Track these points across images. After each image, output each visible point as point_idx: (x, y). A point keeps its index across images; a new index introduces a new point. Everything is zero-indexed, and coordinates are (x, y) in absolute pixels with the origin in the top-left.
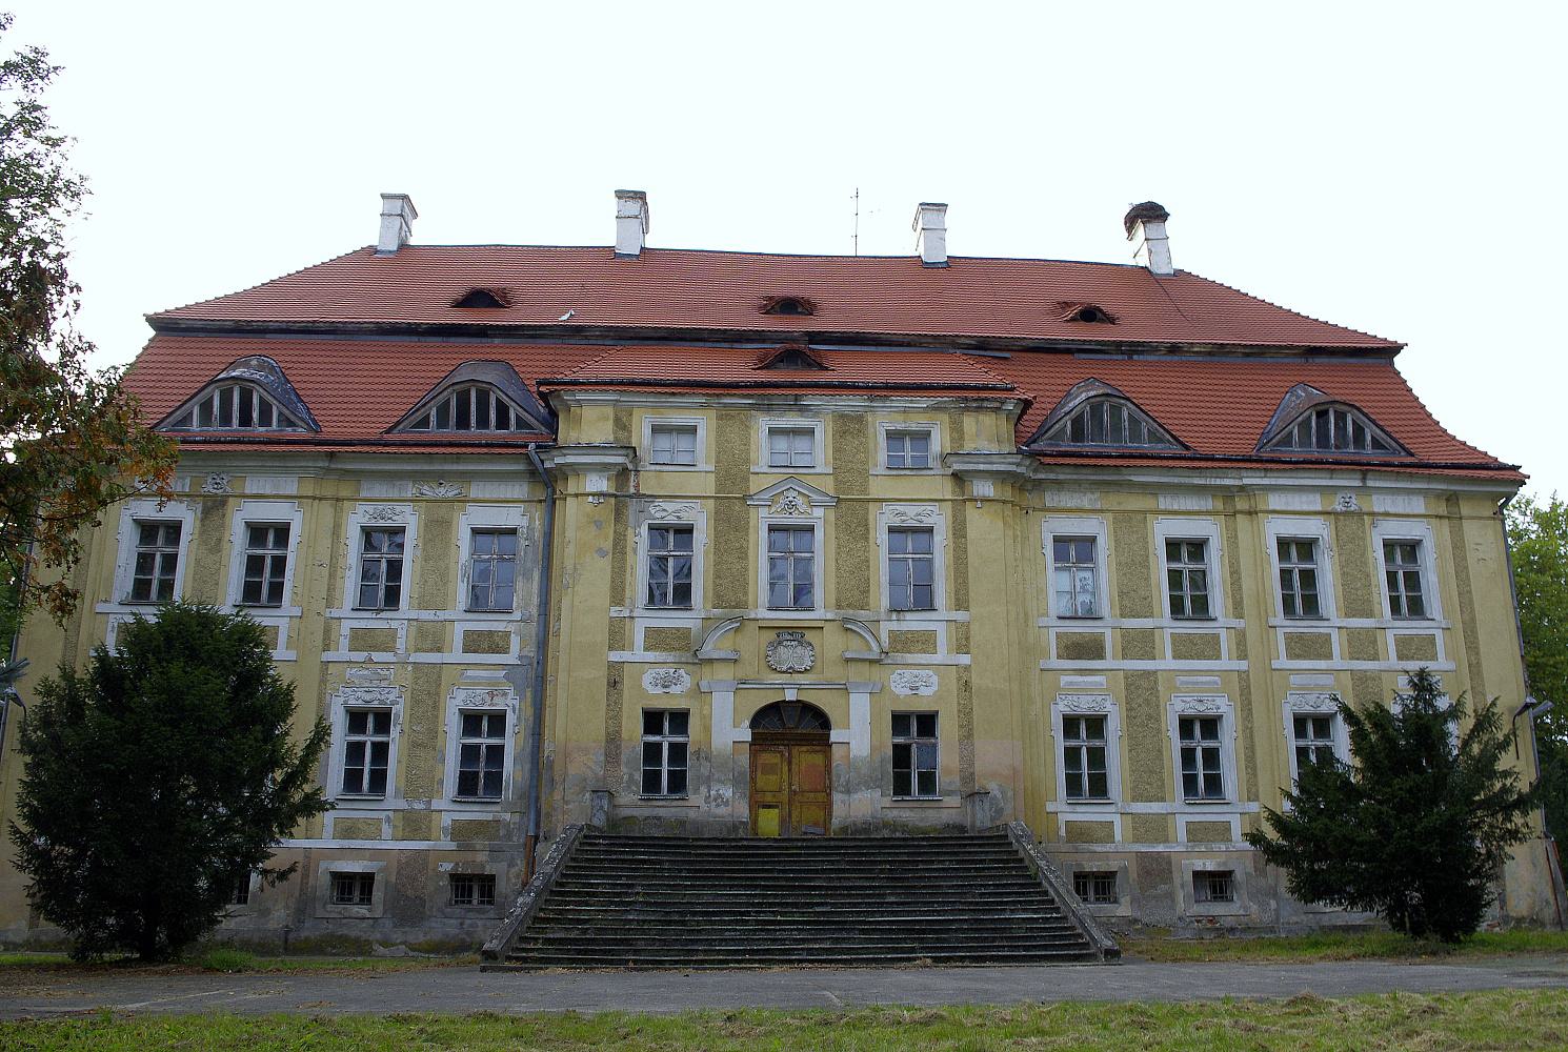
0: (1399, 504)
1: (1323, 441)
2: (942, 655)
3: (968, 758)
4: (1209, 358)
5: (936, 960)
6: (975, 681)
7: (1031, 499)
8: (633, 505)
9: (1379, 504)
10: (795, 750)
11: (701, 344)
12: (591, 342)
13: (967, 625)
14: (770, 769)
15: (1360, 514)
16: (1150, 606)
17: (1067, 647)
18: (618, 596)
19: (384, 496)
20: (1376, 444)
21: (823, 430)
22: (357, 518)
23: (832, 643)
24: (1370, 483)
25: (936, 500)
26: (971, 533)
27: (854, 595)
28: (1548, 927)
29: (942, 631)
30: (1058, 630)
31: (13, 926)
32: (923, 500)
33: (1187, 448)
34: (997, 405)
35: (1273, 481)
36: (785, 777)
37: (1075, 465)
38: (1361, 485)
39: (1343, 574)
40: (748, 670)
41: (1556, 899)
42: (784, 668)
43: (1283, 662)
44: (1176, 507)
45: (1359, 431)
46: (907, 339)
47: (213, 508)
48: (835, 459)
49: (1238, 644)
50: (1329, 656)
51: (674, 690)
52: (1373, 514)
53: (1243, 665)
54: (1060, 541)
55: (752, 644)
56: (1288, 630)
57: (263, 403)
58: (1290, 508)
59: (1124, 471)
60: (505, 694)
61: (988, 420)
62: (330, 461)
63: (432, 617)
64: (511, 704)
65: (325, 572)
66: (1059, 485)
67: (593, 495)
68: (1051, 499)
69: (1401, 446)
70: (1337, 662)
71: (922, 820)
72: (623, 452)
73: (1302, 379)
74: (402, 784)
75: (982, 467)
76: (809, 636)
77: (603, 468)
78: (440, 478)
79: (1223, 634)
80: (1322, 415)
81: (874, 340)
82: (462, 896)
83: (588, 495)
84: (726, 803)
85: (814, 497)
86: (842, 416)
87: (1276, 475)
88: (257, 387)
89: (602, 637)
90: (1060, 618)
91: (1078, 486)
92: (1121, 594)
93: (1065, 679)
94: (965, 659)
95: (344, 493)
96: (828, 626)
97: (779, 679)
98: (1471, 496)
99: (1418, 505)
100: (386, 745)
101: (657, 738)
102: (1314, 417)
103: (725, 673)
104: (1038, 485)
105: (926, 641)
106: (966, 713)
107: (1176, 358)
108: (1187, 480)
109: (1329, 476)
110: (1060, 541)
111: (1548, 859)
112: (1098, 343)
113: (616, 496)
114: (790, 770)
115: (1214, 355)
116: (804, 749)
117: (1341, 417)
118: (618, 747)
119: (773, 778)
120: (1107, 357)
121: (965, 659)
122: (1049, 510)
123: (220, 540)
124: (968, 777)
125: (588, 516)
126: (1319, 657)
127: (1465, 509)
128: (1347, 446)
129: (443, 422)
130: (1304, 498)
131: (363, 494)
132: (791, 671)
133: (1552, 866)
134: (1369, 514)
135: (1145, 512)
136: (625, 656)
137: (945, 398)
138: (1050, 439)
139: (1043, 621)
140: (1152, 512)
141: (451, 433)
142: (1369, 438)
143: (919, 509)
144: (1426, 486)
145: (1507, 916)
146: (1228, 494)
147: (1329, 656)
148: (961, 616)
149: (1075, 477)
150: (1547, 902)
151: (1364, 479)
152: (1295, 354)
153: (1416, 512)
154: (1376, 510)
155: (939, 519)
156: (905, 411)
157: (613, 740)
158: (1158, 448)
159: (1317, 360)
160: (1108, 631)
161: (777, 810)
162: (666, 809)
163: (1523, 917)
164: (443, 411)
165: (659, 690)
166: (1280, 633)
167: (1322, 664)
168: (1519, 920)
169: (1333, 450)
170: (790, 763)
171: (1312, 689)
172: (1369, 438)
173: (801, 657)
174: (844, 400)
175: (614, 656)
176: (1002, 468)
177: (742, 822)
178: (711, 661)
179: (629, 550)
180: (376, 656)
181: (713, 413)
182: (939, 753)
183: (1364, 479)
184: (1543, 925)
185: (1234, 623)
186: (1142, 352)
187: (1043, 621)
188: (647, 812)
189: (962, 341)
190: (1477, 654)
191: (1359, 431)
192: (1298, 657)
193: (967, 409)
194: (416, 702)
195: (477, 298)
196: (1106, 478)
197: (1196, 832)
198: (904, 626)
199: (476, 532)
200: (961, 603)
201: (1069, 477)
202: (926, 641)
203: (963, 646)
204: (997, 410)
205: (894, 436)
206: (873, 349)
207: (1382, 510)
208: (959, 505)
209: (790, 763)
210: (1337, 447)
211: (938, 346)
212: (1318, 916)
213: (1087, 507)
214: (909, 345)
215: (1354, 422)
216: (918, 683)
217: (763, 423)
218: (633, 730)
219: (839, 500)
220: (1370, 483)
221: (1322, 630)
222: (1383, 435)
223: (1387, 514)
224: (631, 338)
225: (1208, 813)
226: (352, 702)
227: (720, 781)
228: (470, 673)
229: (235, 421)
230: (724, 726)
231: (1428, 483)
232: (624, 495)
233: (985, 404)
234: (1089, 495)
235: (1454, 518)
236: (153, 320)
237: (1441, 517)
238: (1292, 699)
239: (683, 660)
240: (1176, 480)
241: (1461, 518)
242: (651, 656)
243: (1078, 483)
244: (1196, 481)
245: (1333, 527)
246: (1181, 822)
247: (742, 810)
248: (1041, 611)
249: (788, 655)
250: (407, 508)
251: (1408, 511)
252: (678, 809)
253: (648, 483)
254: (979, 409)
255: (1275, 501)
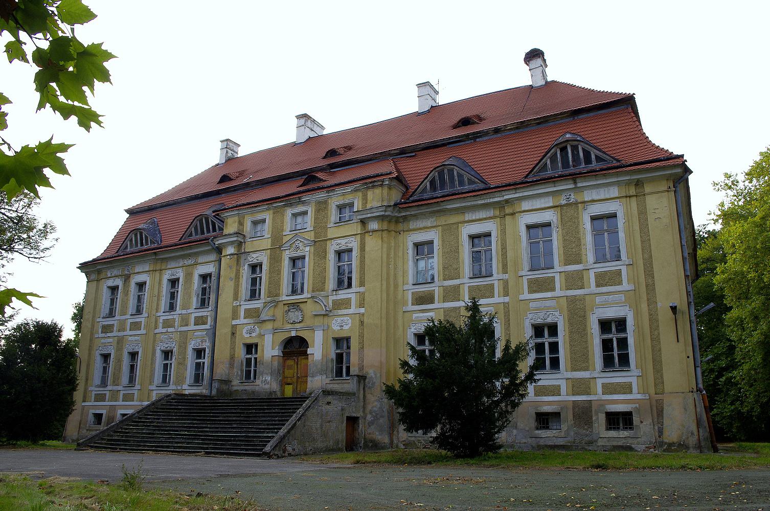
0: (602, 194)
1: (565, 165)
2: (353, 310)
3: (361, 359)
4: (517, 131)
5: (207, 453)
6: (366, 320)
7: (400, 227)
8: (243, 257)
9: (588, 196)
10: (300, 358)
11: (291, 179)
12: (254, 188)
13: (363, 293)
14: (290, 367)
15: (576, 204)
16: (459, 274)
17: (416, 299)
18: (236, 297)
19: (174, 266)
20: (599, 159)
21: (311, 210)
22: (167, 276)
23: (310, 309)
24: (579, 185)
25: (353, 235)
26: (367, 249)
27: (319, 286)
28: (691, 449)
29: (353, 297)
30: (413, 291)
31: (74, 434)
32: (344, 236)
33: (618, 161)
34: (380, 183)
35: (521, 195)
36: (295, 371)
37: (418, 205)
38: (574, 186)
39: (565, 240)
40: (278, 324)
41: (698, 431)
42: (292, 322)
43: (526, 295)
44: (474, 218)
45: (587, 154)
46: (369, 157)
47: (127, 278)
48: (315, 223)
49: (504, 288)
50: (553, 289)
51: (254, 335)
52: (584, 202)
53: (507, 299)
54: (417, 246)
55: (280, 311)
56: (530, 277)
57: (460, 176)
58: (534, 208)
59: (442, 204)
60: (206, 341)
61: (378, 191)
62: (156, 256)
63: (186, 313)
64: (207, 345)
65: (156, 298)
66: (415, 217)
67: (229, 255)
68: (413, 225)
69: (612, 157)
70: (558, 292)
71: (342, 388)
72: (236, 235)
73: (568, 130)
74: (175, 380)
75: (369, 215)
76: (301, 305)
77: (232, 243)
78: (189, 256)
79: (496, 283)
80: (564, 150)
81: (356, 161)
82: (614, 425)
83: (227, 255)
84: (268, 383)
85: (306, 242)
86: (319, 202)
87: (522, 191)
88: (455, 167)
89: (230, 315)
90: (414, 285)
91: (424, 216)
92: (444, 268)
93: (415, 315)
94: (362, 310)
95: (163, 268)
96: (309, 301)
97: (290, 326)
98: (652, 180)
99: (614, 192)
100: (626, 339)
101: (250, 356)
102: (559, 152)
103: (269, 326)
104: (405, 218)
105: (346, 303)
106: (361, 336)
107: (499, 135)
108: (473, 203)
109: (553, 185)
110: (417, 246)
111: (695, 406)
112: (456, 137)
113: (237, 254)
114: (297, 367)
115: (520, 129)
116: (303, 357)
117: (575, 149)
118: (234, 361)
119: (291, 371)
120: (464, 143)
121: (362, 310)
122: (411, 230)
123: (128, 291)
124: (361, 368)
125: (227, 264)
126: (547, 290)
127: (648, 189)
128: (580, 164)
129: (196, 234)
130: (543, 200)
131: (169, 267)
132: (294, 323)
133: (698, 410)
134: (581, 203)
135: (458, 223)
136: (125, 333)
137: (357, 185)
138: (420, 193)
139: (406, 287)
140: (461, 223)
141: (199, 237)
142: (593, 157)
143: (346, 241)
144: (616, 180)
145: (663, 442)
146: (501, 205)
147: (553, 289)
148: (362, 289)
149: (419, 212)
150: (692, 434)
151: (575, 183)
152: (565, 117)
153: (612, 196)
154: (586, 200)
155: (354, 244)
156: (344, 194)
157: (232, 357)
158: (472, 187)
159: (580, 117)
160: (436, 289)
161: (292, 386)
162: (249, 387)
163: (673, 443)
164: (432, 183)
165: (248, 335)
166: (525, 279)
167: (549, 294)
168: (670, 445)
169: (572, 168)
170: (297, 364)
171: (543, 309)
172: (466, 179)
173: (298, 316)
174: (317, 195)
175: (234, 322)
176: (378, 214)
177: (274, 391)
178: (264, 321)
179: (241, 276)
180: (170, 330)
181: (271, 212)
182: (351, 354)
183: (575, 183)
184: (687, 448)
185: (501, 276)
186: (480, 137)
187: (406, 287)
188: (242, 388)
189: (393, 152)
190: (653, 278)
191: (587, 154)
192: (535, 292)
193: (368, 188)
194: (180, 346)
195: (465, 122)
196: (435, 209)
197: (609, 389)
198: (339, 297)
199: (594, 218)
200: (362, 284)
201: (417, 212)
202: (346, 303)
203: (361, 305)
204: (382, 185)
205: (341, 208)
206: (357, 165)
207: (590, 199)
208: (363, 235)
209: (297, 364)
210: (574, 166)
211: (383, 157)
212: (538, 440)
213: (430, 225)
214: (370, 160)
215: (583, 149)
216: (343, 324)
217: (289, 212)
218: (241, 353)
219: (315, 242)
220: (579, 185)
221: (549, 275)
222: (600, 153)
223: (593, 201)
224: (267, 183)
225: (618, 378)
226: (164, 349)
227: (267, 374)
228: (196, 334)
229: (139, 245)
230: (270, 350)
231: (617, 177)
232: (239, 255)
233: (376, 184)
234: (431, 219)
235: (640, 196)
236: (128, 211)
237: (630, 197)
238: (530, 316)
239: (256, 322)
240: (469, 204)
241: (644, 195)
242: (246, 321)
243: (422, 214)
244: (480, 202)
245: (559, 214)
246: (599, 382)
247: (275, 386)
248: (405, 282)
249: (295, 315)
250: (180, 270)
251: (608, 196)
252: (253, 386)
253: (248, 247)
254: (373, 187)
255: (526, 205)
